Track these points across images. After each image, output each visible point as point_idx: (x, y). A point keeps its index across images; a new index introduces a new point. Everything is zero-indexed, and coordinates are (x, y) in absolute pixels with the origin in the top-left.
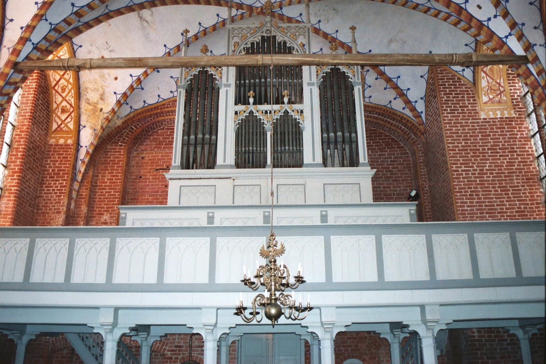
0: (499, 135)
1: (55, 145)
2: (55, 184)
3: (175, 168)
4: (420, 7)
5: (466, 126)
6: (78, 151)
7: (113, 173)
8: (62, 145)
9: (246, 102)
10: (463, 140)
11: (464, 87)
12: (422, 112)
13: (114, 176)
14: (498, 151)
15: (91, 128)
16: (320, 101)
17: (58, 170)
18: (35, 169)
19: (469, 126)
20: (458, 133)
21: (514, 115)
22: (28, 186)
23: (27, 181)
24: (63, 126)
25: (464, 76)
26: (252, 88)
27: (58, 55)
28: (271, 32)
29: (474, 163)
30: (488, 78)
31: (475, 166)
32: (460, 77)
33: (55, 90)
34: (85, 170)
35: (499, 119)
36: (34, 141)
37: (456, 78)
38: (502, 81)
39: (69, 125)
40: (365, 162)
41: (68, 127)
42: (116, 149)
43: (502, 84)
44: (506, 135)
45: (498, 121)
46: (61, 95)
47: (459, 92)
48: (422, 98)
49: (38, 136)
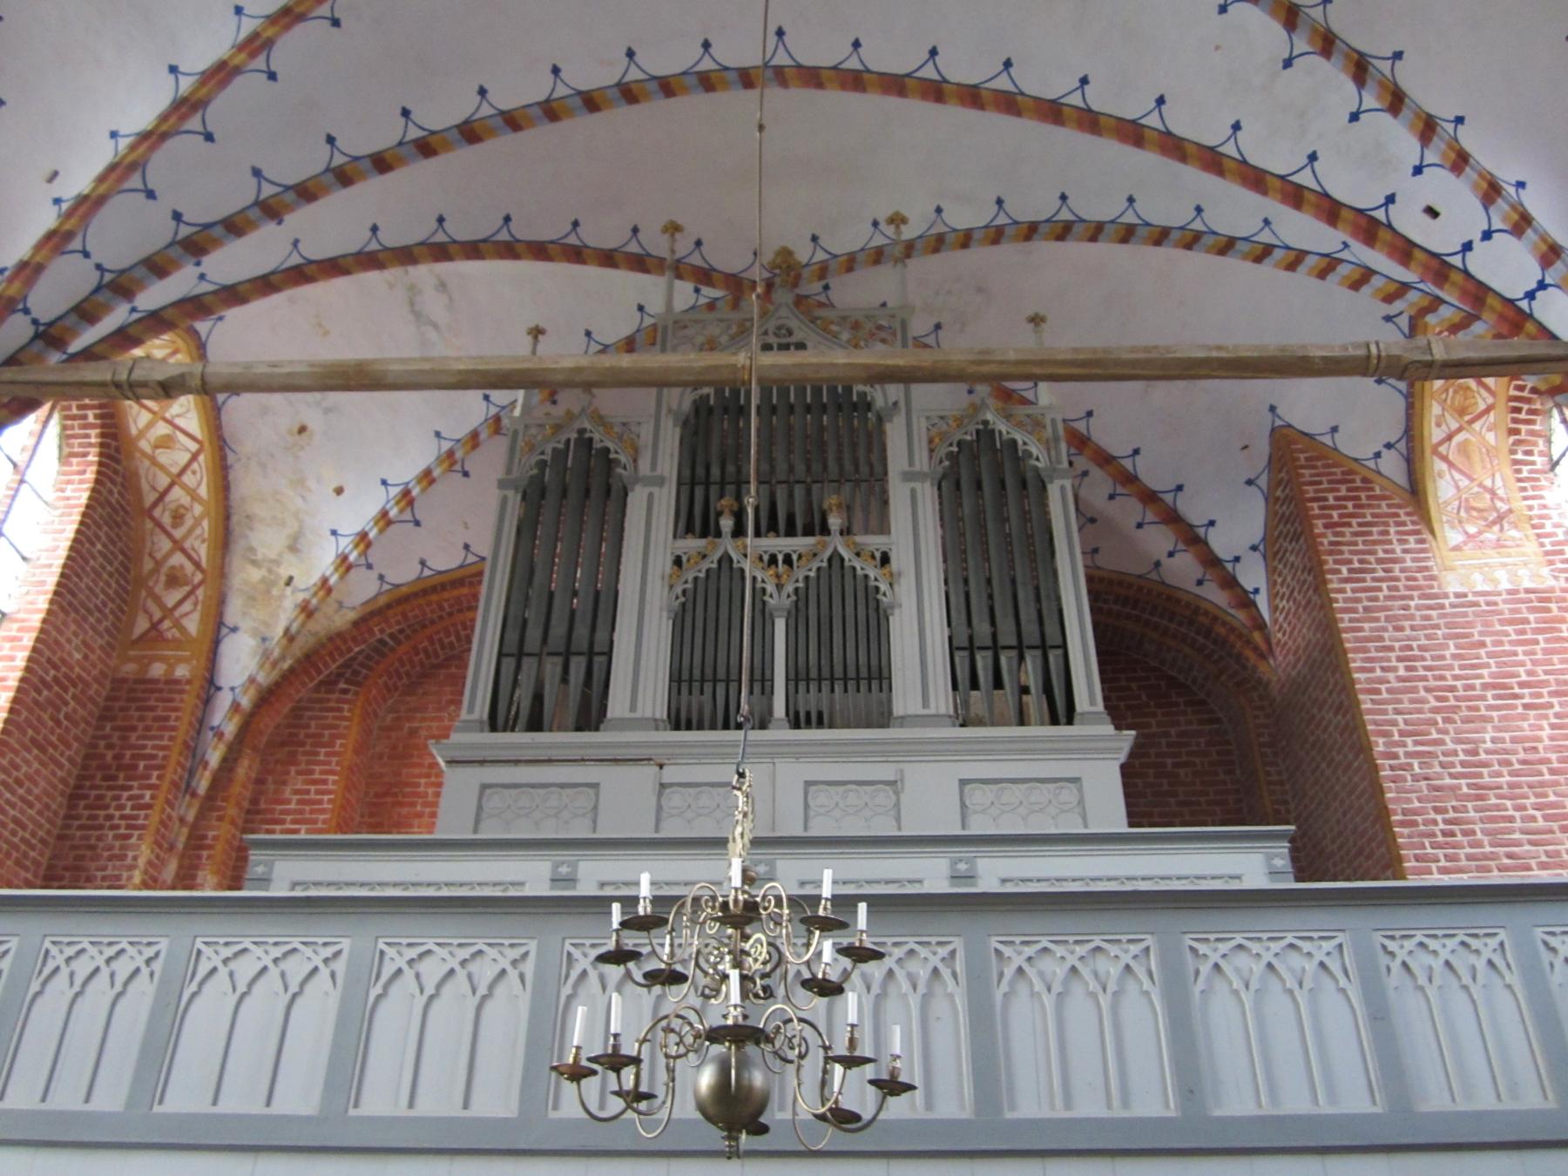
0: (1511, 643)
1: (137, 681)
2: (117, 798)
3: (468, 727)
4: (1240, 246)
5: (1407, 618)
6: (207, 702)
7: (312, 772)
8: (156, 681)
9: (708, 529)
10: (1400, 659)
11: (1384, 503)
12: (1257, 591)
13: (315, 782)
14: (1517, 690)
15: (254, 632)
16: (945, 561)
17: (133, 757)
18: (55, 747)
19: (1412, 618)
20: (1381, 639)
21: (1551, 582)
22: (23, 799)
23: (19, 783)
24: (166, 624)
25: (1379, 473)
26: (730, 488)
27: (168, 415)
28: (790, 333)
29: (1446, 732)
30: (1457, 476)
31: (1447, 739)
32: (1370, 475)
33: (153, 519)
34: (225, 760)
35: (1505, 596)
36: (63, 661)
37: (1358, 478)
38: (1499, 483)
39: (185, 622)
40: (1094, 709)
41: (183, 629)
42: (328, 700)
43: (1501, 492)
44: (1536, 642)
45: (1505, 602)
46: (169, 535)
47: (1369, 519)
48: (1254, 548)
49: (77, 649)
